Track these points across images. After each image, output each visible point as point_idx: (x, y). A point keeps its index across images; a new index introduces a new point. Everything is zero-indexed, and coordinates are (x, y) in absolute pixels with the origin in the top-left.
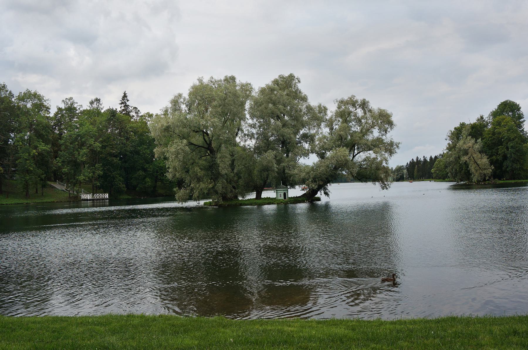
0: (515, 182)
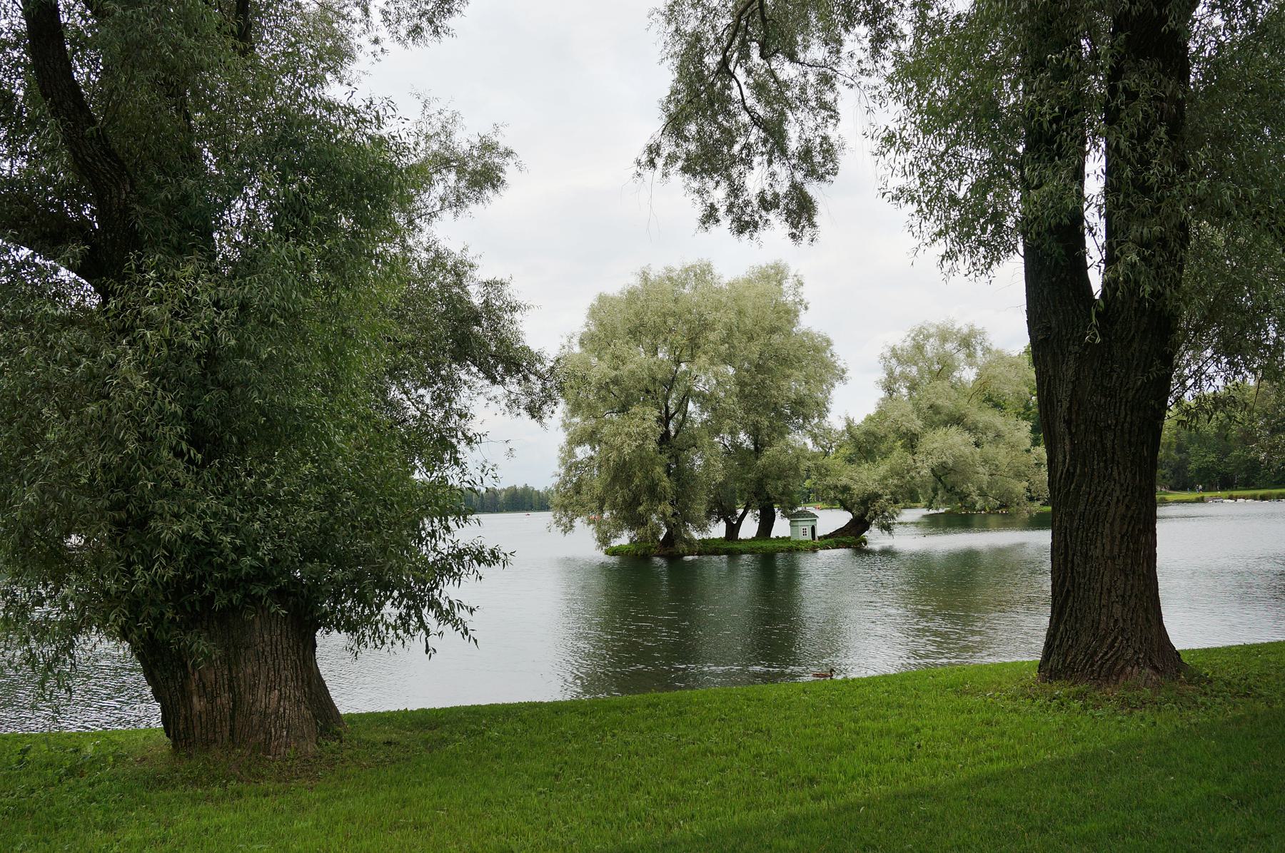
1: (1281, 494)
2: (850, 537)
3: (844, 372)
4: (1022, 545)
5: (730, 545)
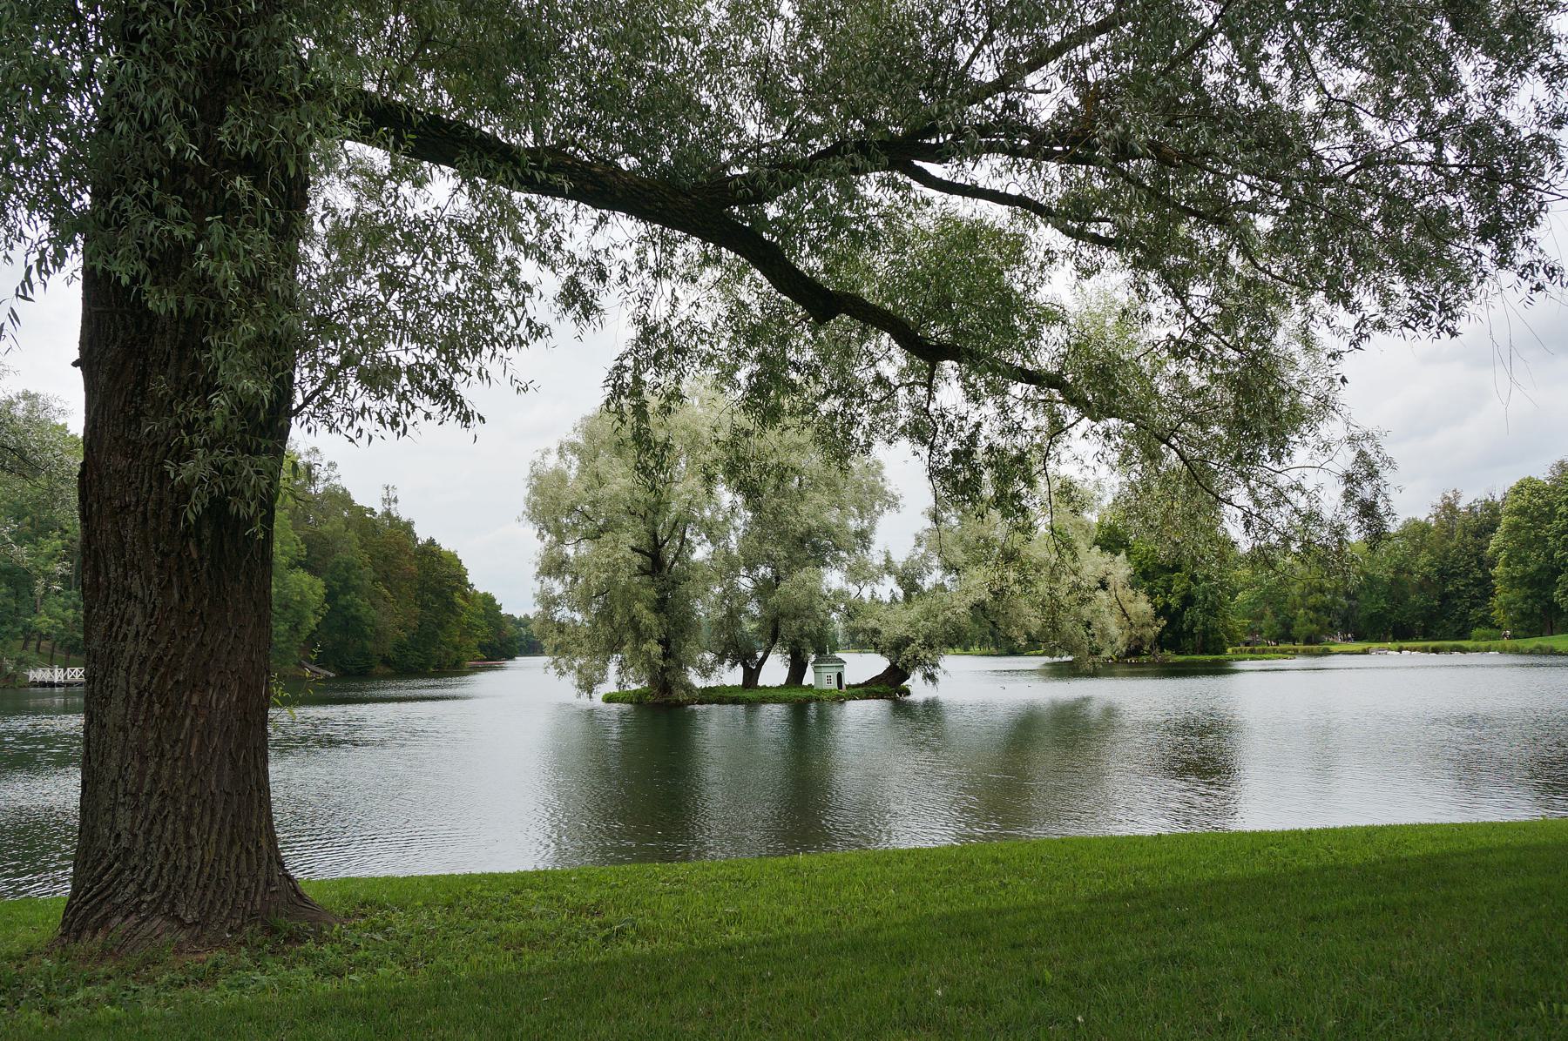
0: (1213, 660)
1: (1455, 646)
2: (889, 685)
3: (896, 498)
4: (1087, 700)
5: (749, 694)
